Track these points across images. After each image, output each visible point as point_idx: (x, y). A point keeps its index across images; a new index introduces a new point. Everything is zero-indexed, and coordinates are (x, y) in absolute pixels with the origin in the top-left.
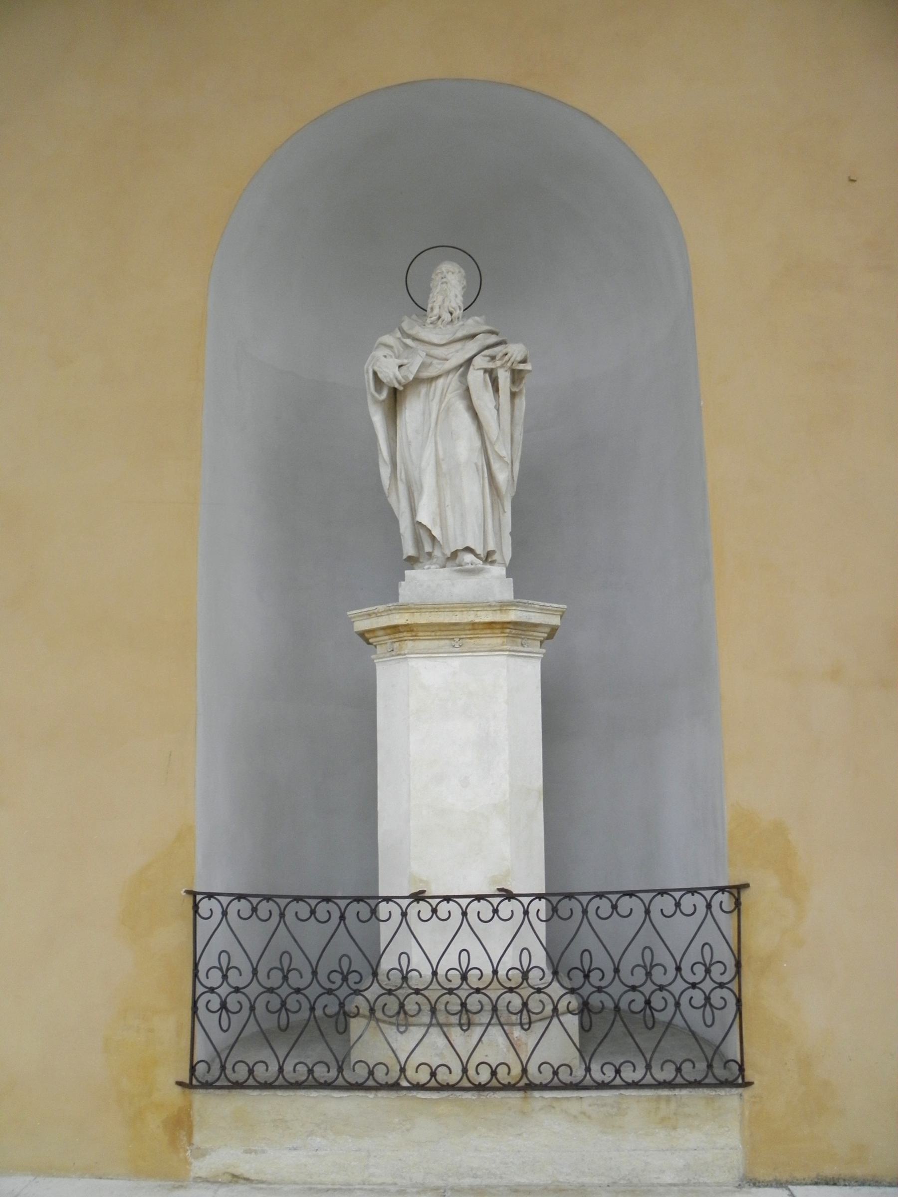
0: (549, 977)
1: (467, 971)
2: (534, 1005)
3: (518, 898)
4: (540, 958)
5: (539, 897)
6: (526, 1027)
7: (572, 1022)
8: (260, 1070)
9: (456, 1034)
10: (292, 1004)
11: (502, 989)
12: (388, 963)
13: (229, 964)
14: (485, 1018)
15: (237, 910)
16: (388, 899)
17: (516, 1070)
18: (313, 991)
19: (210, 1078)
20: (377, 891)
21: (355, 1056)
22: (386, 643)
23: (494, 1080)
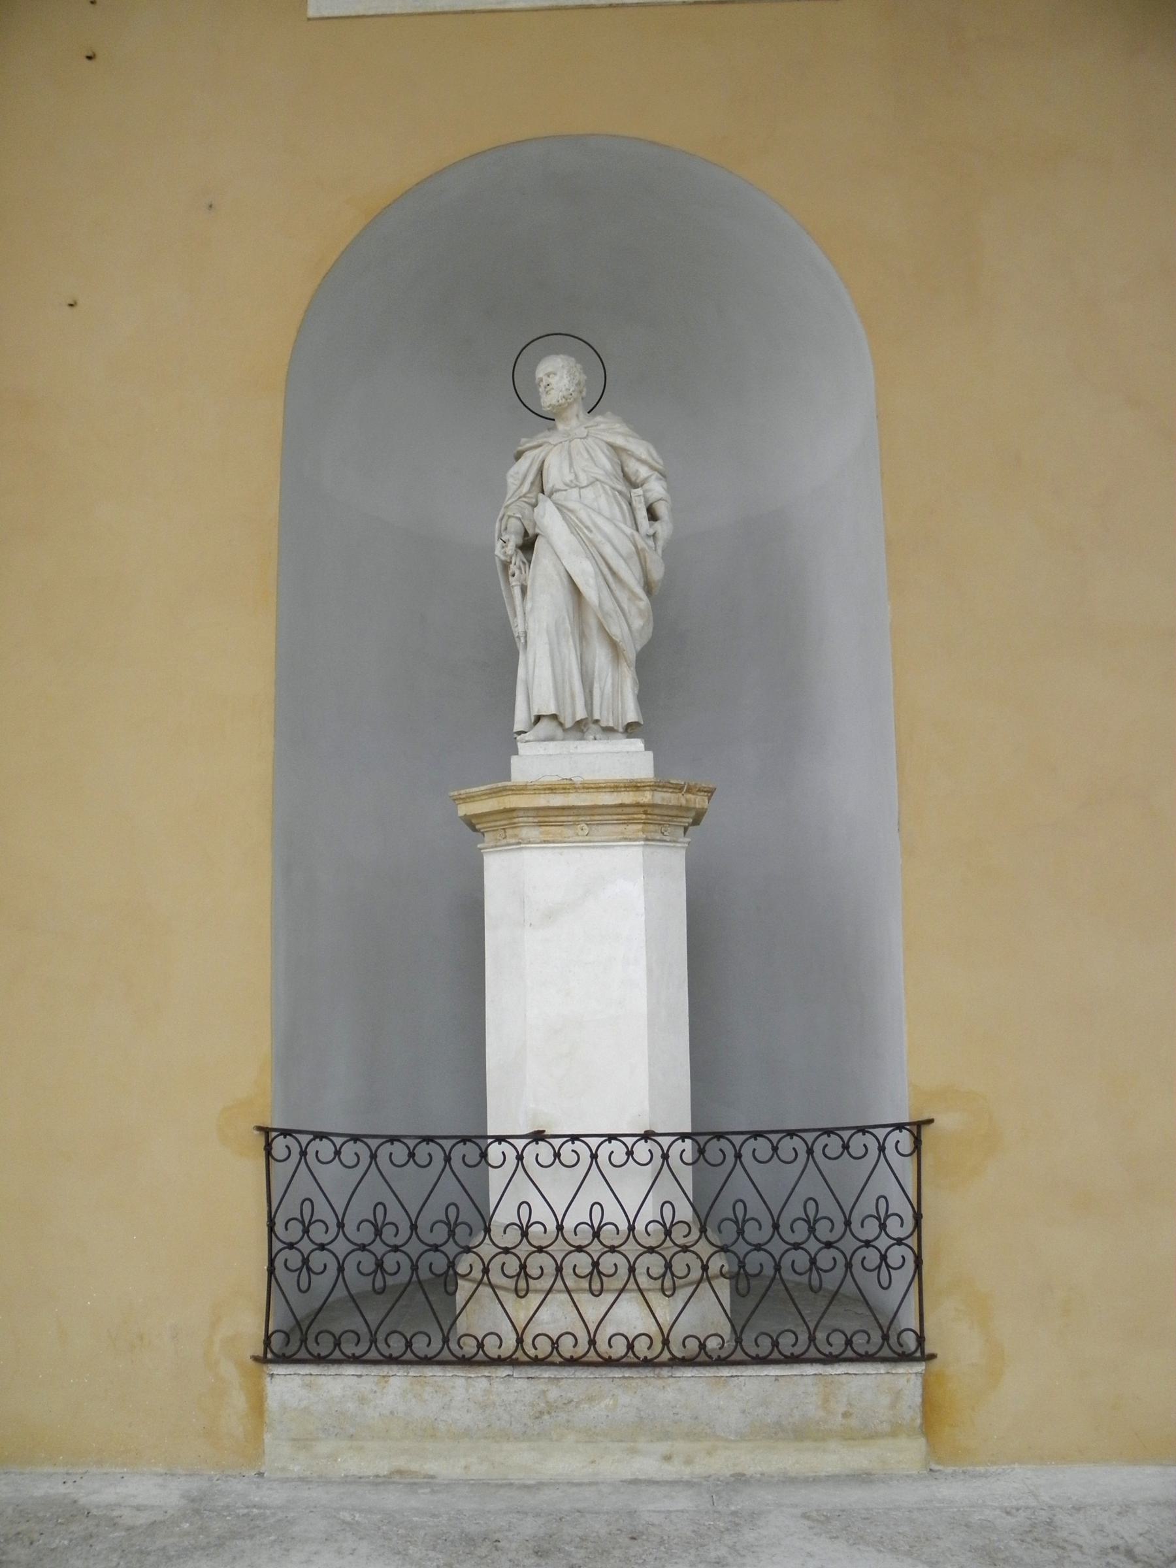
0: (695, 1234)
1: (600, 1228)
2: (679, 1268)
3: (509, 1140)
4: (685, 1212)
5: (683, 1136)
6: (668, 1293)
7: (724, 1288)
8: (859, 1340)
9: (584, 1299)
10: (390, 1263)
11: (625, 1250)
12: (504, 1215)
13: (745, 1215)
14: (545, 1283)
15: (462, 1155)
16: (500, 1139)
17: (510, 1341)
18: (414, 1248)
19: (797, 1350)
20: (487, 1133)
21: (462, 1326)
22: (497, 830)
23: (630, 1354)
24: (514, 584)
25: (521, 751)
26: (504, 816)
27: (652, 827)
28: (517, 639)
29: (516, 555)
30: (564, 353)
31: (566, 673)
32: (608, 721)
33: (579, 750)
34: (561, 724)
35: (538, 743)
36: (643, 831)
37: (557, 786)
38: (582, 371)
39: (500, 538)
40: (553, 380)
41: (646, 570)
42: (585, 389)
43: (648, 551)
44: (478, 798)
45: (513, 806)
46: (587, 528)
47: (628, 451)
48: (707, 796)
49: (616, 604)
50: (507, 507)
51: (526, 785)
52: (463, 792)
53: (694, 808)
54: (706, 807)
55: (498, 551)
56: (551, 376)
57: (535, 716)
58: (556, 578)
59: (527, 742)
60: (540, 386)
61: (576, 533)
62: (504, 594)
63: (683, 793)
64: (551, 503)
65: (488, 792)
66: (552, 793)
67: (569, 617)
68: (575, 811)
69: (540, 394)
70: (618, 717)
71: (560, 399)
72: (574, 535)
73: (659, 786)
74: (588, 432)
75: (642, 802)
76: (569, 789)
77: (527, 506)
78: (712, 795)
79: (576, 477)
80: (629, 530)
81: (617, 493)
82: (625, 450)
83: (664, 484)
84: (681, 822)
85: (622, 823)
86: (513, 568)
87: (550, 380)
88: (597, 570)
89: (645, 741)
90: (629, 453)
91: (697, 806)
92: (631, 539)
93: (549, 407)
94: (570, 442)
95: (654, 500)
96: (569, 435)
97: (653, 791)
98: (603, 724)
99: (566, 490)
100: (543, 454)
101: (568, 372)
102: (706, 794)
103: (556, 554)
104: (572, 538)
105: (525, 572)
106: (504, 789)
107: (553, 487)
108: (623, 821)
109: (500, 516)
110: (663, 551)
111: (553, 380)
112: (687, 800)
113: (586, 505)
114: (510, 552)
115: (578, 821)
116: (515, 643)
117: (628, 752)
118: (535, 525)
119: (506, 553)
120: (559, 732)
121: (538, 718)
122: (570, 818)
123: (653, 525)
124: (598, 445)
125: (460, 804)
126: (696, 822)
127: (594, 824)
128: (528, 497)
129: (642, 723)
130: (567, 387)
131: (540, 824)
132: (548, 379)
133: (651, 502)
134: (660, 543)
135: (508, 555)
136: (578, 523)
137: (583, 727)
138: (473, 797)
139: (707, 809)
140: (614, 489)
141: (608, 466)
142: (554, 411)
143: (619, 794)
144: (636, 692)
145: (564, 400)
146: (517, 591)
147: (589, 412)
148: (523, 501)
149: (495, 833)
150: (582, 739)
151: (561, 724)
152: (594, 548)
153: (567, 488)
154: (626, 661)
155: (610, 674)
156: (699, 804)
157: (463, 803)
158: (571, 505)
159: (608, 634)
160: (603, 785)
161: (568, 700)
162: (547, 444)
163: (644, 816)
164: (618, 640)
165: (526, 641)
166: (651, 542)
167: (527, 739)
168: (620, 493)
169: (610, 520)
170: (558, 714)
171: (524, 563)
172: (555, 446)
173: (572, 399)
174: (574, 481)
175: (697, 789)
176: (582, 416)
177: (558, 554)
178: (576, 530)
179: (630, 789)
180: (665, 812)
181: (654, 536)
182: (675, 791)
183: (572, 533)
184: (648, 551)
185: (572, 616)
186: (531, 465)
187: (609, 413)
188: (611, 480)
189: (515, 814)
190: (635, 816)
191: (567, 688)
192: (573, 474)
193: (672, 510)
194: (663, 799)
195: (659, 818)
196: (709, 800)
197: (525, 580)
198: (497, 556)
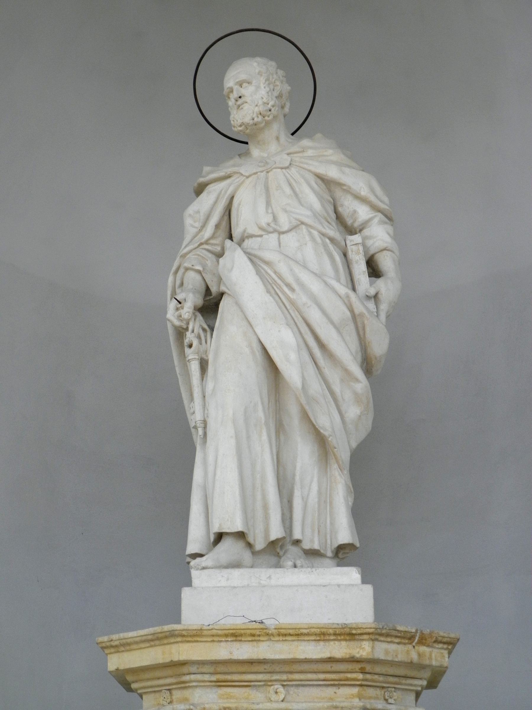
22: (161, 691)
24: (190, 357)
25: (196, 581)
26: (169, 672)
27: (371, 692)
28: (193, 430)
29: (195, 320)
30: (261, 56)
31: (258, 476)
32: (312, 541)
33: (273, 582)
34: (250, 545)
35: (217, 571)
36: (360, 697)
37: (242, 632)
38: (284, 79)
39: (174, 293)
40: (247, 91)
41: (365, 343)
42: (288, 105)
43: (368, 316)
44: (135, 647)
45: (183, 657)
46: (288, 285)
47: (344, 185)
48: (447, 649)
49: (325, 387)
50: (184, 256)
51: (201, 630)
52: (115, 637)
53: (430, 666)
54: (445, 664)
55: (171, 314)
56: (244, 85)
57: (214, 533)
58: (247, 350)
59: (204, 568)
60: (229, 98)
61: (273, 292)
62: (178, 370)
63: (414, 644)
64: (242, 253)
65: (150, 637)
66: (236, 641)
67: (262, 403)
68: (267, 667)
69: (229, 109)
70: (326, 536)
71: (255, 116)
72: (271, 295)
73: (381, 635)
74: (291, 160)
75: (358, 656)
76: (259, 636)
77: (210, 255)
78: (453, 648)
79: (275, 219)
80: (343, 290)
81: (328, 241)
82: (339, 185)
83: (390, 229)
84: (411, 685)
85: (332, 685)
86: (189, 337)
87: (243, 91)
88: (301, 340)
89: (362, 571)
90: (345, 188)
91: (434, 663)
92: (346, 301)
93: (240, 126)
94: (268, 172)
95: (376, 251)
96: (267, 163)
97: (373, 640)
98: (306, 545)
99: (261, 236)
100: (231, 189)
101: (267, 80)
102: (445, 646)
103: (247, 319)
104: (268, 298)
105: (206, 342)
106: (172, 634)
107: (245, 231)
108: (332, 683)
109: (174, 268)
110: (388, 317)
111: (247, 91)
112: (419, 655)
113: (287, 256)
114: (186, 316)
115: (271, 681)
116: (191, 434)
117: (339, 586)
118: (220, 280)
119: (181, 316)
120: (247, 556)
121: (220, 537)
122: (260, 677)
123: (375, 282)
124: (303, 177)
125: (111, 653)
126: (432, 684)
127: (292, 686)
128: (213, 244)
129: (358, 545)
130: (265, 100)
131: (219, 684)
132: (240, 88)
133: (372, 252)
134: (384, 307)
135: (184, 319)
136: (276, 278)
137: (278, 550)
138: (129, 644)
139: (447, 667)
140: (323, 235)
141: (317, 205)
142: (248, 131)
143: (327, 644)
144: (350, 504)
145: (260, 118)
146: (195, 367)
147: (293, 134)
148: (203, 249)
149: (157, 695)
150: (278, 566)
151: (250, 545)
152: (297, 313)
153: (263, 233)
154: (337, 462)
155: (315, 479)
156: (436, 660)
157: (116, 652)
158: (268, 255)
159: (313, 425)
160: (305, 631)
161: (260, 513)
162: (239, 175)
163: (361, 676)
164: (326, 434)
165: (205, 434)
166: (371, 305)
167: (204, 564)
168: (332, 240)
169: (320, 276)
170: (245, 531)
171: (204, 330)
172: (248, 177)
173: (271, 117)
174: (272, 225)
175: (434, 639)
176: (283, 138)
177: (250, 319)
178: (273, 288)
179: (342, 637)
180: (391, 671)
181: (376, 297)
182: (403, 641)
183: (268, 292)
184: (368, 316)
185: (266, 400)
186: (216, 202)
187: (319, 135)
188: (321, 223)
189: (185, 669)
190: (349, 675)
191: (259, 497)
192: (271, 215)
193: (400, 264)
194: (387, 652)
195: (381, 678)
196: (450, 653)
197: (206, 352)
198: (169, 320)
